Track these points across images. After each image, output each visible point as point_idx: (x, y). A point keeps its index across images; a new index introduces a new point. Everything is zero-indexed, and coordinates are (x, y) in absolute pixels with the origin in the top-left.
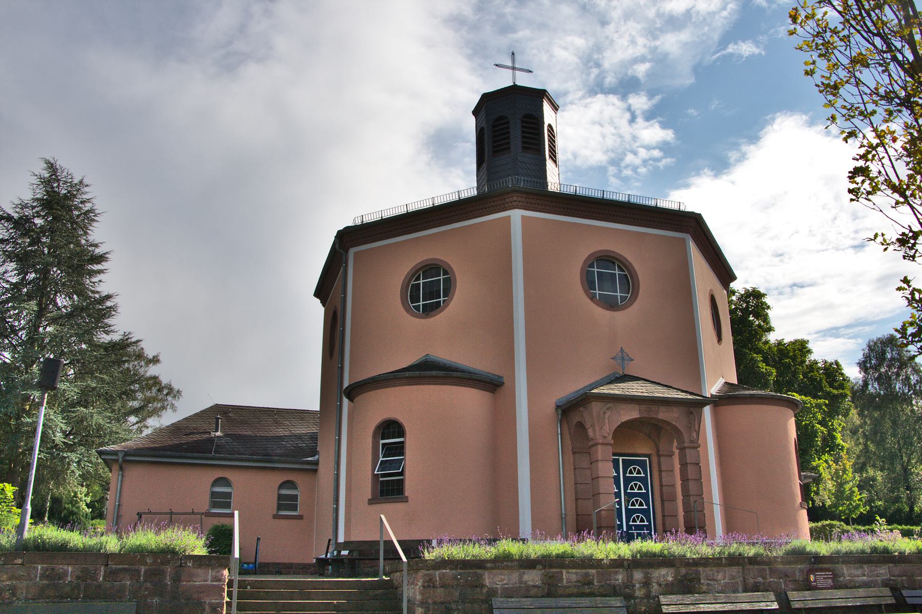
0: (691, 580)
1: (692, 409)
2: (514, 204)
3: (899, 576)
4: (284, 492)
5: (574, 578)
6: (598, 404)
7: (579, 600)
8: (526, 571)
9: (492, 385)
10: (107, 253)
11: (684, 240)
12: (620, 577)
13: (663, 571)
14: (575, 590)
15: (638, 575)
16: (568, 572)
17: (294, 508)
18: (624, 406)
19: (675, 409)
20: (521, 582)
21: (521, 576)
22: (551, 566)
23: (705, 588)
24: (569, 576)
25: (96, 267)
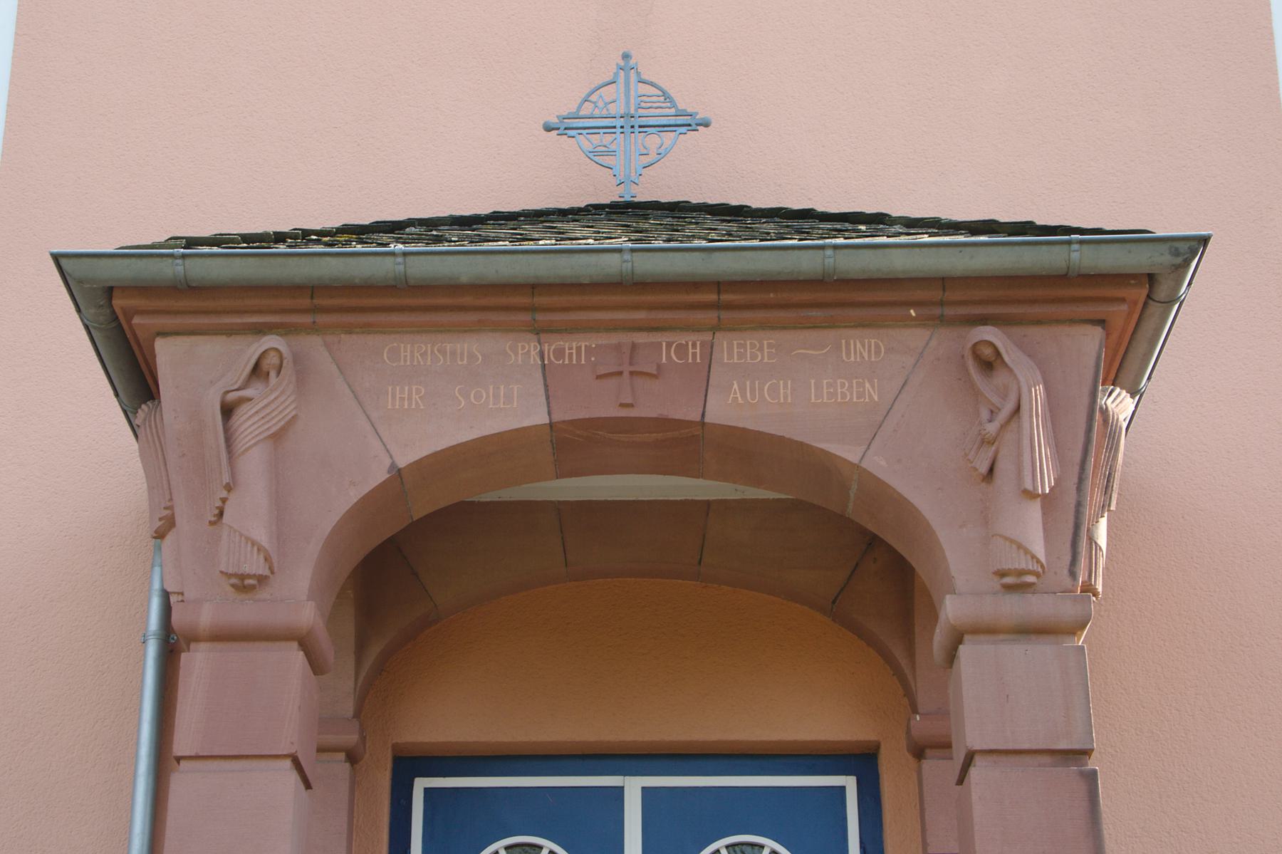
19: (861, 346)
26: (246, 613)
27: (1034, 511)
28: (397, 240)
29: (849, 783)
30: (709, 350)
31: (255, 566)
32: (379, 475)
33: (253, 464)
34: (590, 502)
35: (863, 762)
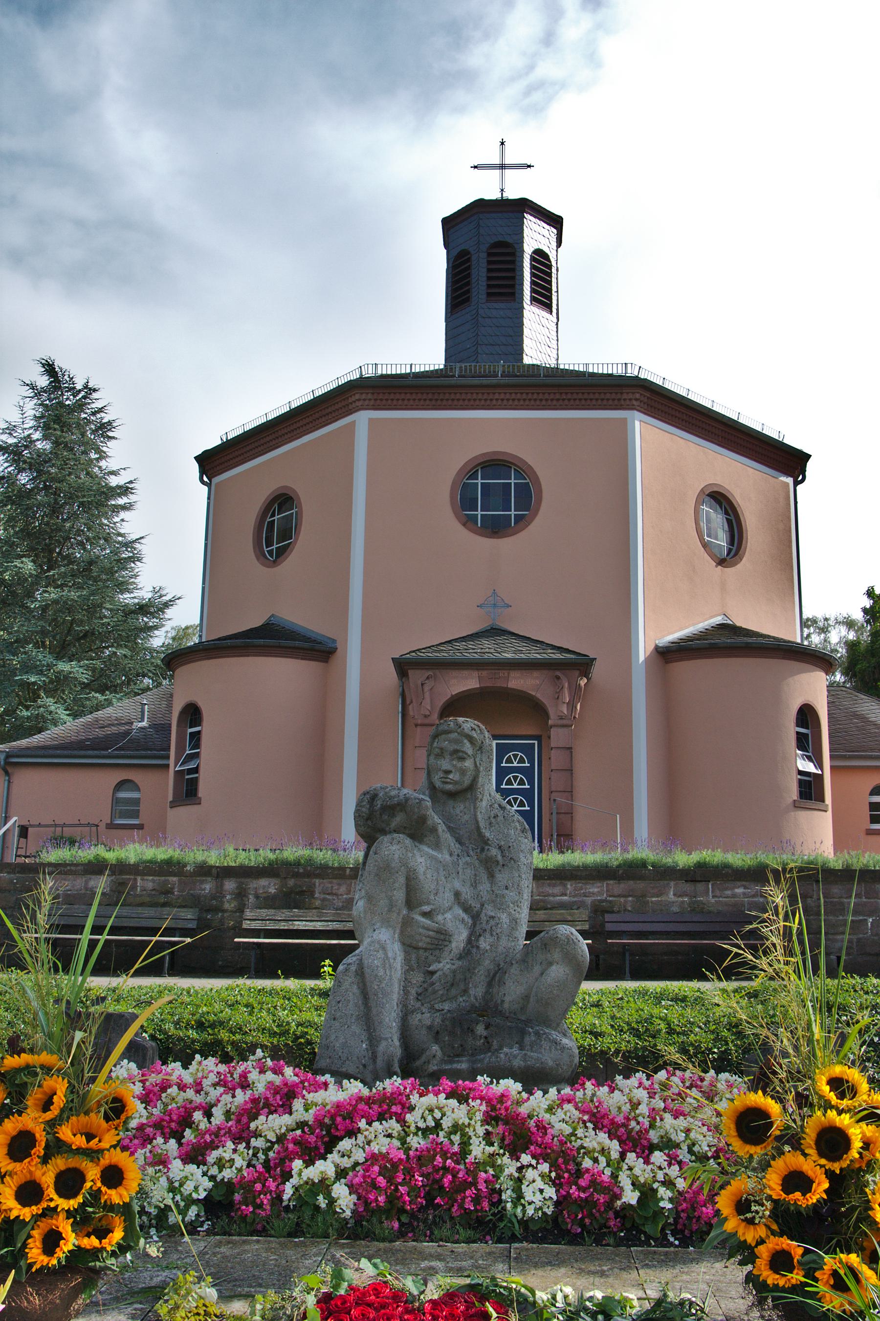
0: (302, 893)
1: (558, 673)
2: (358, 404)
3: (619, 896)
4: (122, 795)
5: (150, 885)
6: (418, 672)
7: (140, 910)
8: (93, 877)
9: (321, 651)
10: (131, 482)
11: (624, 421)
12: (208, 887)
13: (263, 882)
14: (148, 899)
15: (230, 885)
16: (142, 880)
17: (135, 814)
18: (455, 673)
19: (536, 674)
20: (86, 889)
21: (87, 882)
22: (121, 872)
23: (318, 903)
24: (145, 884)
25: (121, 501)
26: (427, 721)
27: (565, 705)
28: (752, 954)
29: (536, 742)
30: (509, 673)
31: (428, 713)
32: (449, 696)
33: (427, 695)
34: (633, 809)
35: (538, 738)
